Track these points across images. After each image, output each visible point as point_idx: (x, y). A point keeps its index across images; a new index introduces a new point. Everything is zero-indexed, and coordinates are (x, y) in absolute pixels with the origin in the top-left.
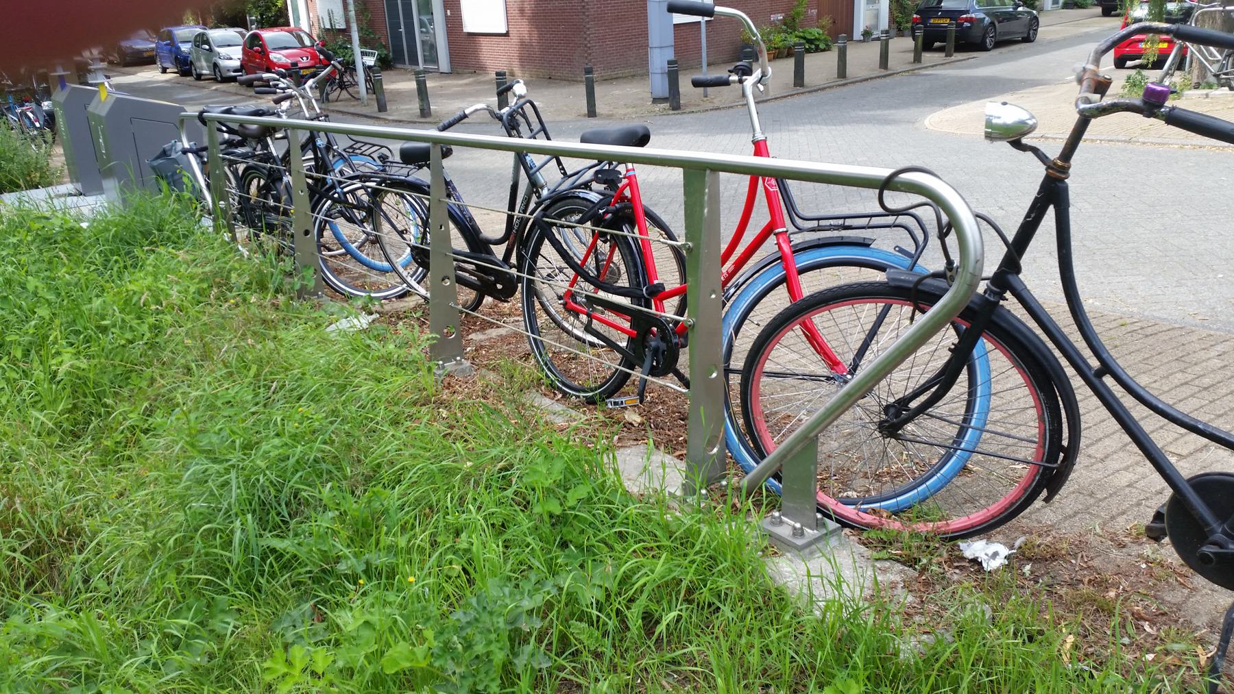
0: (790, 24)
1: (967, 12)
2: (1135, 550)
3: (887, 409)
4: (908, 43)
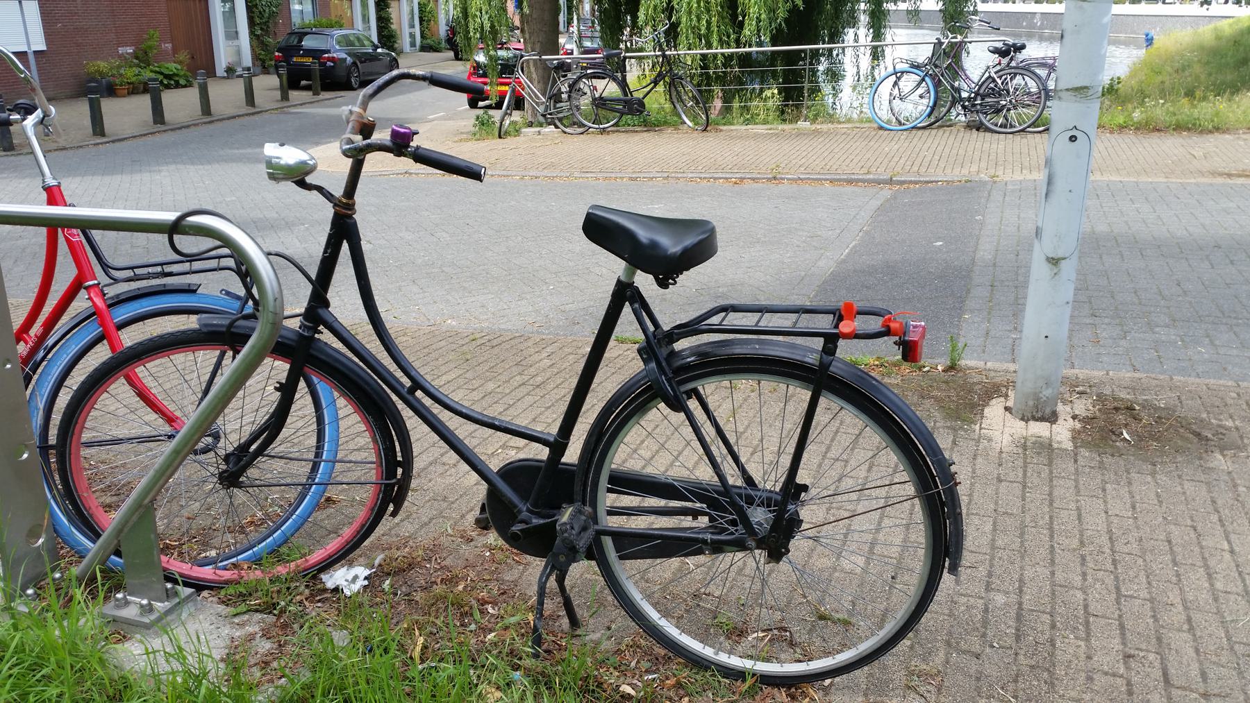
0: (143, 58)
1: (328, 51)
2: (481, 541)
3: (227, 458)
4: (273, 80)
